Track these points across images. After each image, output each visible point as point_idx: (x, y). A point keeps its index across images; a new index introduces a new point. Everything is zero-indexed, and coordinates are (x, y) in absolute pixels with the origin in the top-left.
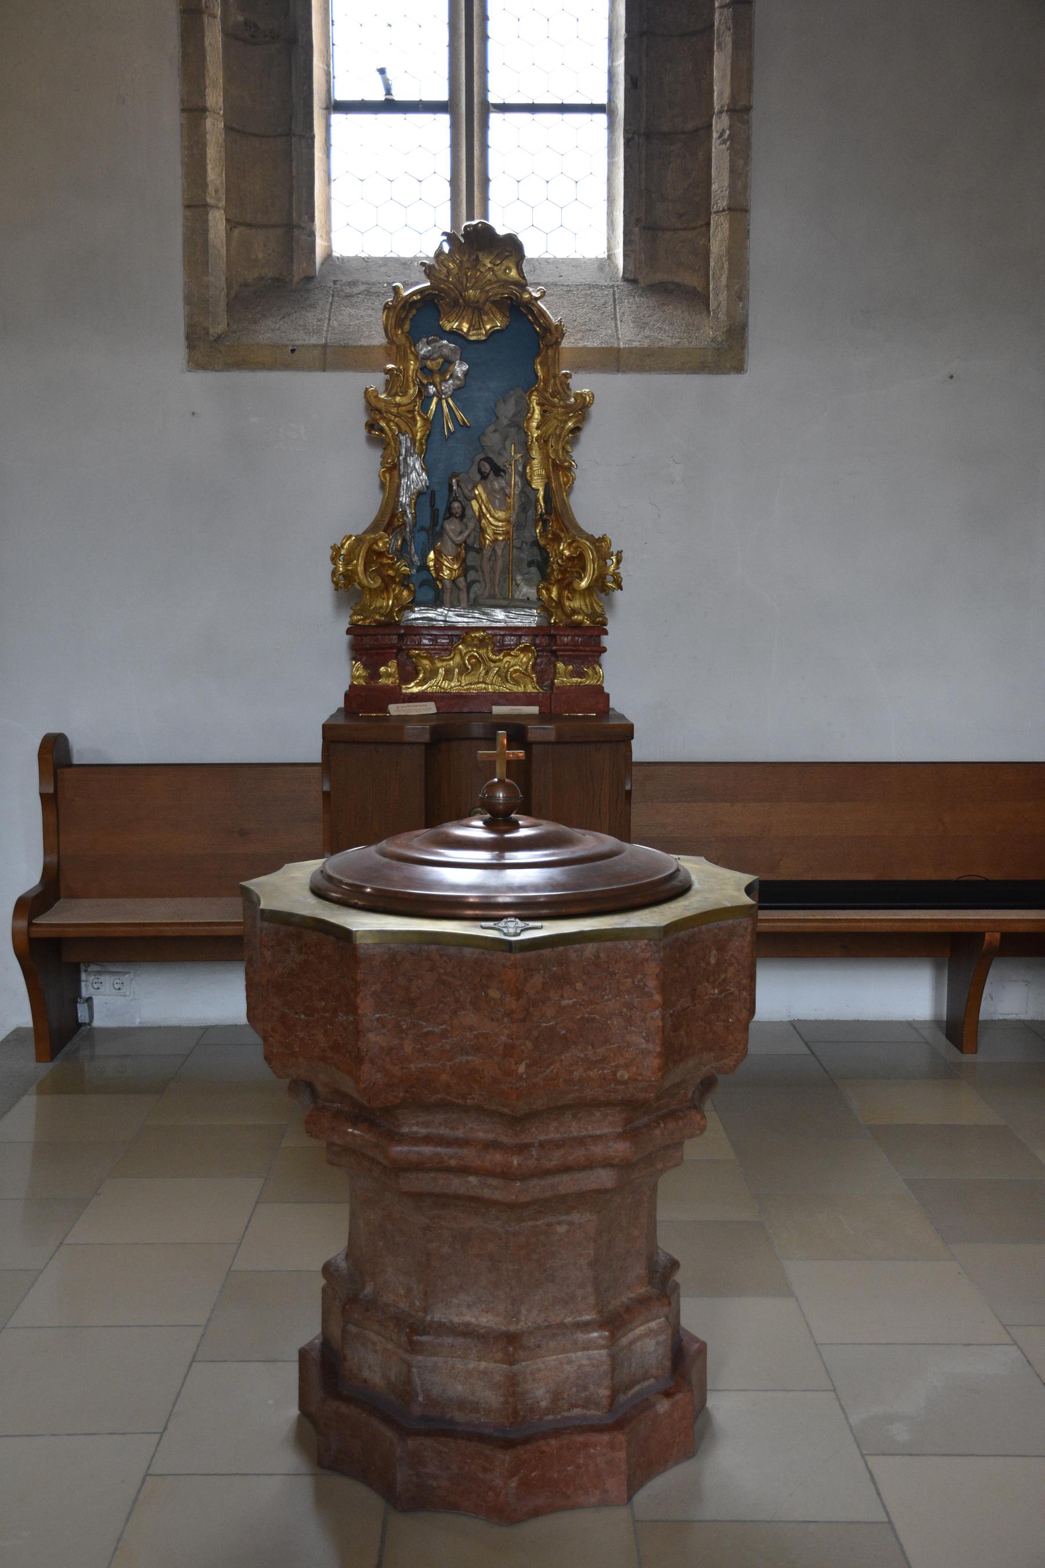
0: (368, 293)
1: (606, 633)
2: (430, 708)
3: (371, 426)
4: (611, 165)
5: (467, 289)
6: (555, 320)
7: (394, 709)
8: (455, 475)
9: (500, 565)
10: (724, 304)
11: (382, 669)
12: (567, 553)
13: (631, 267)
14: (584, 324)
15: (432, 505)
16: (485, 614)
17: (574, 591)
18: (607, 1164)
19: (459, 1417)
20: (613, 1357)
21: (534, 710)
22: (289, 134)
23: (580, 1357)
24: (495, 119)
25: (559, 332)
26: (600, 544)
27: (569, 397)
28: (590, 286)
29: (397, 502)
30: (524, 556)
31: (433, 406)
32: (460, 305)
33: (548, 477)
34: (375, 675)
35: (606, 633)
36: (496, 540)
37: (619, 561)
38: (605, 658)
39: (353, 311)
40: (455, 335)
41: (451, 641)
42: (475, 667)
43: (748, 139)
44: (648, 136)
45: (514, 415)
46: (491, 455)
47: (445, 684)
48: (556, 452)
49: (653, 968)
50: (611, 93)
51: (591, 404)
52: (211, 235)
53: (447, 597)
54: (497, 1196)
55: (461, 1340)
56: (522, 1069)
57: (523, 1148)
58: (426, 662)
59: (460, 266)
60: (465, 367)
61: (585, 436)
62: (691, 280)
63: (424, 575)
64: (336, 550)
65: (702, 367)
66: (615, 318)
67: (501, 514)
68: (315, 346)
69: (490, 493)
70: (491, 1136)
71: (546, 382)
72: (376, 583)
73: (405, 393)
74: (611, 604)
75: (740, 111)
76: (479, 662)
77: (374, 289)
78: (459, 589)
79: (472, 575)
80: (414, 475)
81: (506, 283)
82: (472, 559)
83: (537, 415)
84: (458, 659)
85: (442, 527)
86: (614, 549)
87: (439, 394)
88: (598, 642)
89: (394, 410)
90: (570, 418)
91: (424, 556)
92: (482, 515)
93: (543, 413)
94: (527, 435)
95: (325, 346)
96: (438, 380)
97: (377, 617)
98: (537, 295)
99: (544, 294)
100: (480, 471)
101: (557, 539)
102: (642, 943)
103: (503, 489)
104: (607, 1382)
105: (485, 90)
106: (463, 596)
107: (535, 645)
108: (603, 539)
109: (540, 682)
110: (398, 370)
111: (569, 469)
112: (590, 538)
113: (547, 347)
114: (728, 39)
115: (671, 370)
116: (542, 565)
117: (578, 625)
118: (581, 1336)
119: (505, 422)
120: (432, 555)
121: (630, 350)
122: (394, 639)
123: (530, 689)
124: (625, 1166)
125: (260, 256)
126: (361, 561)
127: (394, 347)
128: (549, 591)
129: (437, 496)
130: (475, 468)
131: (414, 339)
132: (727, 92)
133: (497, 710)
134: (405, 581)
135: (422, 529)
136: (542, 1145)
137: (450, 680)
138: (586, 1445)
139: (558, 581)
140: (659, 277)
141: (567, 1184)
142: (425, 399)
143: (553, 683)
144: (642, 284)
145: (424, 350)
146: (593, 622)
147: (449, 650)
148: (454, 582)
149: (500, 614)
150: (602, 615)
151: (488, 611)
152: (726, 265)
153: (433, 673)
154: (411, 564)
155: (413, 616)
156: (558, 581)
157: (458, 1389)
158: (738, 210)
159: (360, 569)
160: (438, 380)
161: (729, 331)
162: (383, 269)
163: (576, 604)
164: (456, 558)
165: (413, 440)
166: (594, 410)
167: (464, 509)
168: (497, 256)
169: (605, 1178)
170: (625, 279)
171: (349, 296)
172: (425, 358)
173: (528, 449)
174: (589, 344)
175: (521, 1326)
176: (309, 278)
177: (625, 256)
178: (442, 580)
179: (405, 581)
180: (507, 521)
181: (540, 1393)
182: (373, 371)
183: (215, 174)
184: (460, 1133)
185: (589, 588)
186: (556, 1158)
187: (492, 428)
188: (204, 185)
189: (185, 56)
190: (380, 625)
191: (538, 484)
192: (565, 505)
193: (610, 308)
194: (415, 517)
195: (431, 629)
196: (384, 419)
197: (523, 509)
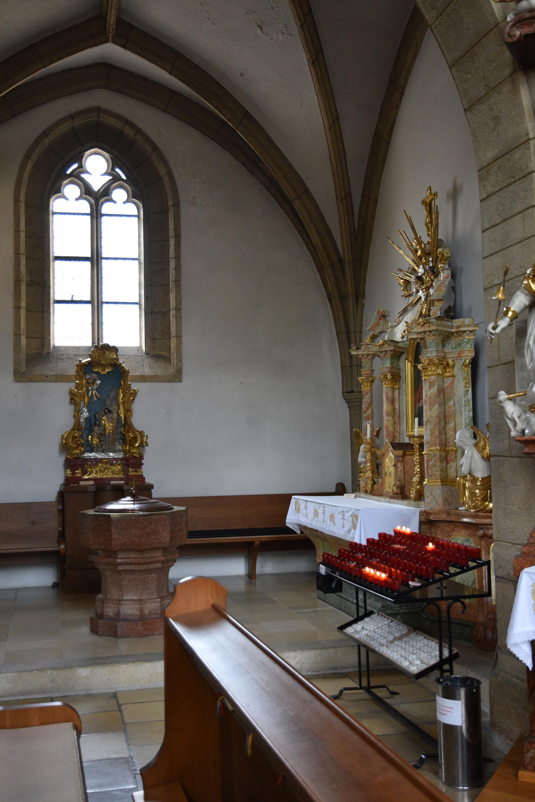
0: (68, 358)
1: (143, 459)
2: (92, 482)
3: (72, 399)
4: (140, 320)
5: (101, 361)
6: (127, 369)
7: (82, 483)
8: (97, 413)
9: (111, 440)
10: (175, 362)
11: (77, 471)
12: (132, 436)
13: (147, 350)
14: (134, 368)
15: (90, 422)
16: (106, 454)
17: (134, 447)
18: (159, 562)
19: (130, 618)
20: (161, 605)
21: (123, 482)
22: (43, 311)
23: (155, 605)
24: (104, 306)
25: (128, 372)
26: (141, 433)
27: (131, 390)
28: (135, 356)
29: (80, 422)
30: (118, 437)
31: (90, 393)
32: (99, 364)
33: (125, 413)
34: (74, 473)
35: (143, 459)
36: (109, 432)
37: (147, 438)
38: (143, 467)
39: (63, 364)
40: (97, 373)
41: (97, 463)
42: (105, 470)
43: (181, 317)
44: (151, 313)
45: (115, 396)
46: (108, 407)
47: (96, 476)
48: (127, 406)
49: (168, 520)
50: (140, 300)
51: (137, 392)
52: (22, 343)
53: (95, 450)
54: (138, 569)
55: (130, 602)
56: (144, 539)
57: (143, 558)
58: (89, 469)
59: (99, 354)
60: (100, 382)
61: (135, 401)
62: (165, 354)
63: (87, 443)
64: (63, 436)
65: (170, 381)
66: (143, 366)
67: (111, 425)
68: (53, 375)
69: (108, 418)
70: (137, 556)
71: (124, 386)
72: (75, 446)
73: (82, 389)
74: (144, 450)
75: (178, 309)
76: (105, 469)
77: (69, 357)
78: (98, 447)
79: (102, 443)
80: (85, 413)
81: (113, 359)
82: (102, 438)
83: (122, 395)
84: (99, 468)
85: (93, 429)
86: (145, 434)
87: (92, 390)
88: (141, 462)
89: (79, 395)
90: (131, 397)
91: (88, 437)
92: (105, 425)
93: (123, 395)
94: (118, 401)
95: (56, 375)
96: (92, 385)
97: (75, 456)
98: (122, 362)
99: (124, 362)
100: (104, 412)
101: (129, 432)
102: (166, 516)
103: (112, 417)
104: (160, 609)
105: (102, 298)
106: (100, 449)
107: (123, 463)
108: (142, 432)
109: (124, 474)
110: (80, 383)
111: (131, 411)
112: (138, 431)
113: (125, 376)
114: (174, 290)
115: (160, 381)
116: (124, 440)
117: (135, 457)
118: (155, 600)
119: (112, 397)
120: (90, 437)
121: (149, 376)
122: (80, 463)
123: (121, 476)
124: (163, 562)
125: (34, 346)
126: (71, 439)
127: (78, 377)
128: (126, 447)
129: (92, 420)
130: (103, 411)
131: (85, 374)
132: (174, 304)
133: (112, 482)
134: (82, 445)
135: (87, 429)
136: (147, 557)
137: (97, 474)
138: (156, 621)
139: (129, 444)
140: (156, 353)
141: (151, 566)
142: (88, 391)
143: (128, 474)
144: (151, 355)
145: (88, 377)
146: (140, 456)
147: (96, 465)
148: (97, 445)
149: (111, 454)
150: (142, 454)
151: (107, 453)
152: (176, 352)
153: (91, 472)
154: (84, 440)
155: (85, 455)
156: (129, 444)
157: (130, 612)
158: (179, 336)
159: (70, 442)
160: (92, 385)
161: (177, 370)
162: (71, 350)
163: (134, 451)
164: (98, 438)
165: (84, 403)
166: (138, 394)
167: (100, 423)
168: (110, 351)
169: (159, 565)
170: (146, 353)
171: (62, 359)
172: (88, 379)
173: (118, 405)
174: (136, 374)
175: (143, 598)
176: (49, 353)
177: (145, 347)
178: (93, 444)
179: (82, 445)
180: (113, 427)
181: (147, 612)
182: (71, 382)
183: (23, 325)
184: (130, 556)
185: (138, 446)
186: (149, 560)
187: (108, 399)
188: (20, 329)
189: (15, 293)
190: (76, 458)
191: (122, 416)
192: (130, 421)
193: (142, 363)
194: (85, 426)
195: (90, 459)
196: (76, 397)
197: (118, 423)
